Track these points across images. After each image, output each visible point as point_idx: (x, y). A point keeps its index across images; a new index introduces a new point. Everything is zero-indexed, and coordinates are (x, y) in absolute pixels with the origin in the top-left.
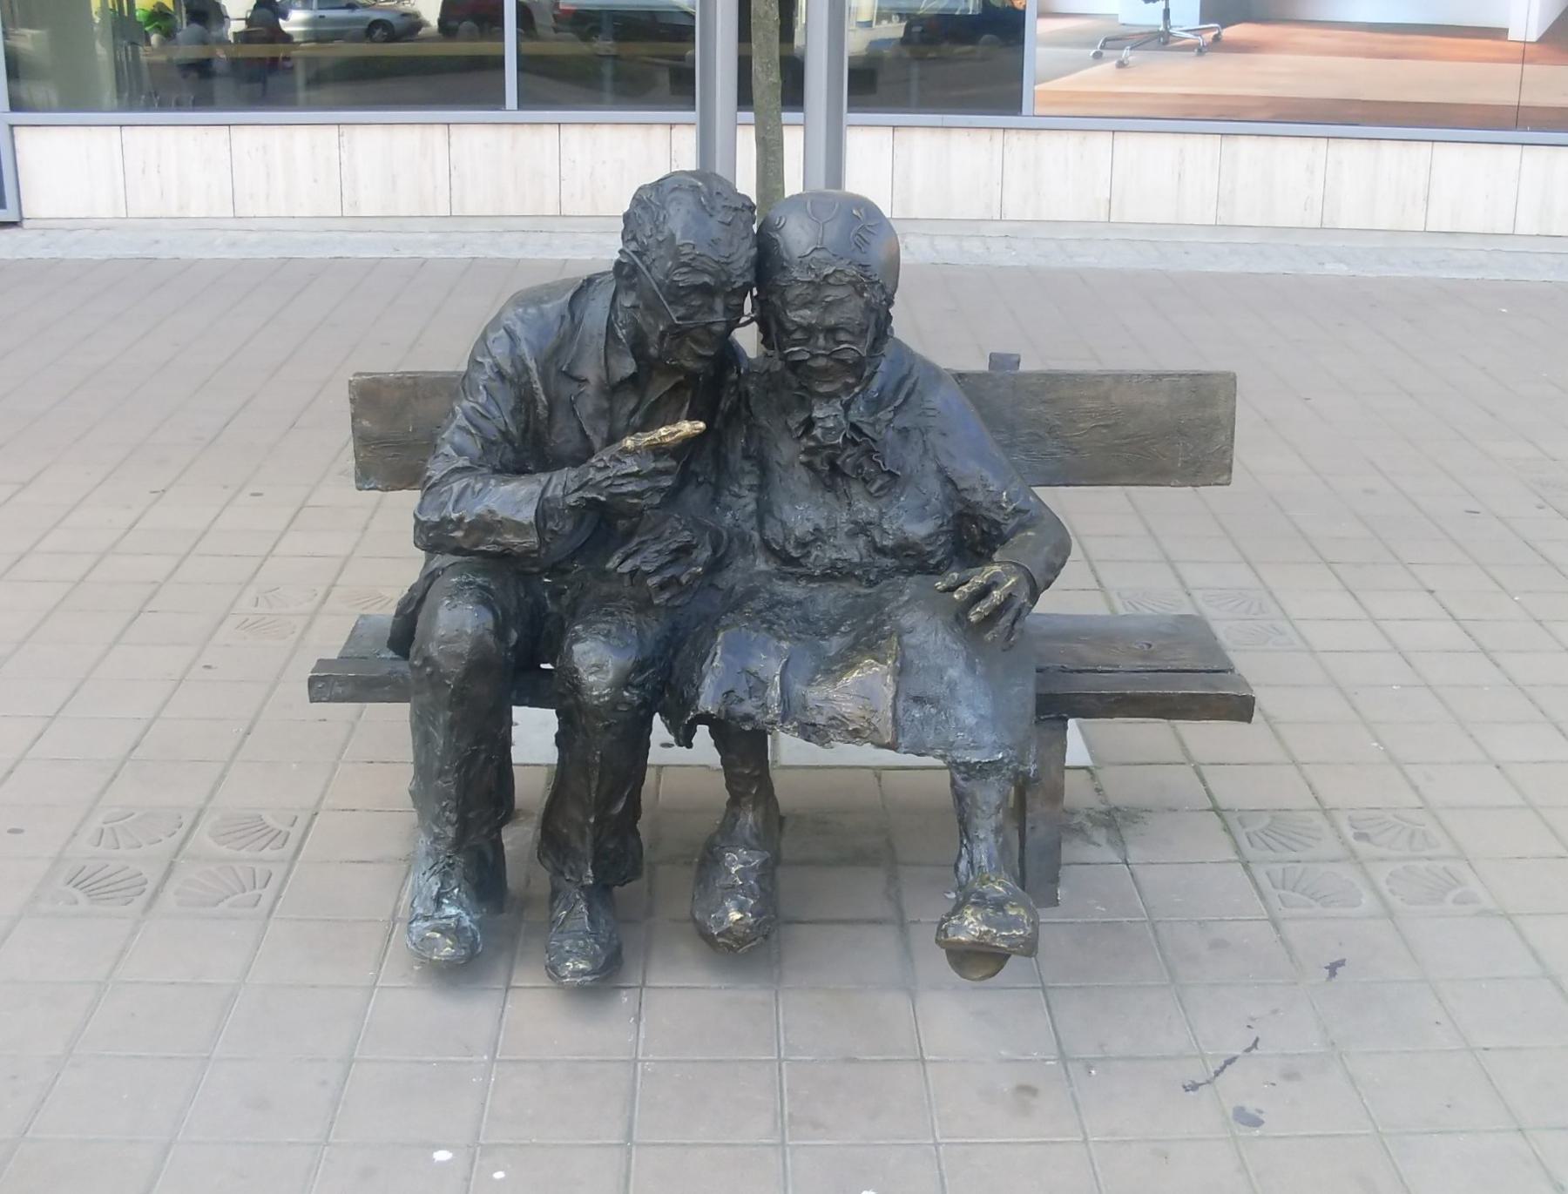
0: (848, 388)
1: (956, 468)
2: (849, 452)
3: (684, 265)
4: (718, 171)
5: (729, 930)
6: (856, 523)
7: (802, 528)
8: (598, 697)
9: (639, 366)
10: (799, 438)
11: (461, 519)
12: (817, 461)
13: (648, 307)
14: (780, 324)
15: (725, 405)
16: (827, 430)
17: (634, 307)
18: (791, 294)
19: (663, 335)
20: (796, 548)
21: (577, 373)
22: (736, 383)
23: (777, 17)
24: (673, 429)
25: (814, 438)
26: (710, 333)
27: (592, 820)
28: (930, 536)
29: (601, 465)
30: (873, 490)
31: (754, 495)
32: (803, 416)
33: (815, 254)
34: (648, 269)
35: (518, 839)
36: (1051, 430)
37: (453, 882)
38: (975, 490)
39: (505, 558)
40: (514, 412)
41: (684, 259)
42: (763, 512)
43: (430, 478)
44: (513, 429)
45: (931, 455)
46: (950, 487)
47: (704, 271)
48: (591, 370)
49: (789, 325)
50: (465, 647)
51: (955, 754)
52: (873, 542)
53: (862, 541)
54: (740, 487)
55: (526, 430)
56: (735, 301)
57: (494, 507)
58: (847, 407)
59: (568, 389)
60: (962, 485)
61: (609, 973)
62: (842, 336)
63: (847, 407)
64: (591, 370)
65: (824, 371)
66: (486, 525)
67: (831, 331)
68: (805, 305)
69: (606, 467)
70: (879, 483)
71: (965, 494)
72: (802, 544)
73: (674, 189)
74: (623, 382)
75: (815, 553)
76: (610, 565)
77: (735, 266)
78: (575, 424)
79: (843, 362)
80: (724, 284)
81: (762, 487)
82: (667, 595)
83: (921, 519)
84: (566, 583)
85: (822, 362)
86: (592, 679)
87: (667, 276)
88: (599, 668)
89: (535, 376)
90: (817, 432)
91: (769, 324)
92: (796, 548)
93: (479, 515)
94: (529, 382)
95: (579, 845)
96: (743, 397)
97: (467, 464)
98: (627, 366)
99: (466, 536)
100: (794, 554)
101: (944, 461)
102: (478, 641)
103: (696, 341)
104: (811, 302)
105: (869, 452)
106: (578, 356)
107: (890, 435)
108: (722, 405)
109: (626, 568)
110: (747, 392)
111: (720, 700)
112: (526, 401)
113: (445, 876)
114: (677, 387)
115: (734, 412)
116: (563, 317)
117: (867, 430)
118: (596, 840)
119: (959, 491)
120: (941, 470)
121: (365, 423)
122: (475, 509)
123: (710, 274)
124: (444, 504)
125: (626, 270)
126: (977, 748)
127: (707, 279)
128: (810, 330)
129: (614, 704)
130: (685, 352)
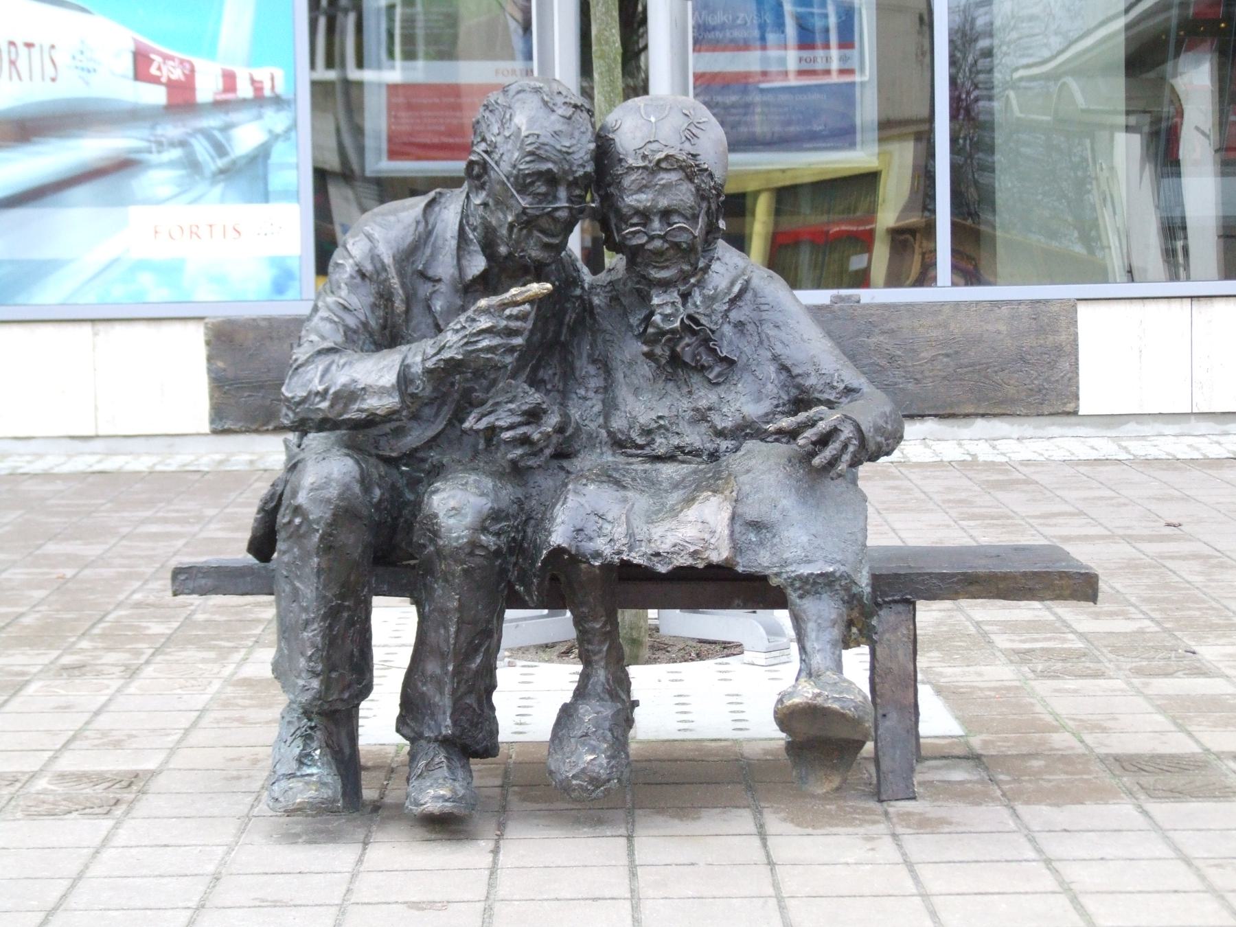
0: (685, 277)
1: (791, 354)
2: (687, 340)
3: (531, 153)
4: (557, 77)
5: (583, 770)
6: (697, 410)
7: (645, 418)
8: (458, 538)
11: (326, 391)
12: (658, 350)
13: (497, 203)
14: (618, 211)
15: (570, 318)
16: (666, 317)
17: (485, 205)
18: (626, 182)
19: (511, 227)
20: (641, 435)
21: (431, 273)
22: (580, 297)
23: (618, 44)
24: (523, 289)
27: (450, 668)
28: (767, 414)
29: (459, 326)
30: (711, 376)
31: (600, 396)
33: (649, 146)
34: (497, 163)
35: (378, 723)
36: (892, 359)
37: (315, 745)
38: (808, 375)
39: (371, 421)
40: (374, 307)
41: (529, 148)
42: (610, 407)
43: (296, 360)
44: (373, 323)
45: (766, 343)
46: (785, 373)
47: (547, 160)
48: (444, 268)
50: (333, 492)
51: (788, 569)
52: (713, 427)
53: (704, 427)
54: (587, 389)
55: (384, 327)
56: (577, 192)
57: (357, 376)
58: (685, 296)
59: (425, 289)
60: (795, 371)
62: (675, 218)
63: (685, 296)
64: (444, 268)
65: (659, 253)
66: (349, 395)
67: (666, 214)
68: (641, 190)
69: (464, 328)
70: (717, 370)
71: (799, 380)
72: (647, 432)
73: (518, 92)
74: (476, 280)
75: (658, 440)
76: (467, 425)
77: (576, 156)
78: (430, 321)
79: (677, 245)
80: (565, 173)
81: (607, 389)
82: (519, 452)
83: (758, 400)
84: (423, 471)
85: (658, 243)
86: (452, 521)
87: (514, 166)
88: (456, 511)
89: (392, 271)
90: (657, 318)
91: (609, 225)
92: (641, 435)
93: (344, 385)
94: (387, 279)
95: (437, 699)
96: (588, 309)
97: (332, 345)
98: (477, 264)
99: (332, 406)
100: (640, 441)
101: (779, 349)
102: (347, 487)
103: (543, 232)
104: (645, 186)
105: (706, 341)
106: (433, 256)
107: (727, 329)
108: (567, 319)
109: (482, 425)
110: (591, 303)
111: (570, 534)
112: (385, 297)
113: (307, 738)
115: (580, 321)
116: (418, 223)
117: (703, 320)
118: (454, 691)
119: (793, 377)
120: (775, 358)
121: (220, 364)
122: (340, 379)
123: (554, 162)
124: (310, 381)
125: (476, 169)
126: (809, 562)
127: (550, 165)
128: (645, 215)
129: (474, 545)
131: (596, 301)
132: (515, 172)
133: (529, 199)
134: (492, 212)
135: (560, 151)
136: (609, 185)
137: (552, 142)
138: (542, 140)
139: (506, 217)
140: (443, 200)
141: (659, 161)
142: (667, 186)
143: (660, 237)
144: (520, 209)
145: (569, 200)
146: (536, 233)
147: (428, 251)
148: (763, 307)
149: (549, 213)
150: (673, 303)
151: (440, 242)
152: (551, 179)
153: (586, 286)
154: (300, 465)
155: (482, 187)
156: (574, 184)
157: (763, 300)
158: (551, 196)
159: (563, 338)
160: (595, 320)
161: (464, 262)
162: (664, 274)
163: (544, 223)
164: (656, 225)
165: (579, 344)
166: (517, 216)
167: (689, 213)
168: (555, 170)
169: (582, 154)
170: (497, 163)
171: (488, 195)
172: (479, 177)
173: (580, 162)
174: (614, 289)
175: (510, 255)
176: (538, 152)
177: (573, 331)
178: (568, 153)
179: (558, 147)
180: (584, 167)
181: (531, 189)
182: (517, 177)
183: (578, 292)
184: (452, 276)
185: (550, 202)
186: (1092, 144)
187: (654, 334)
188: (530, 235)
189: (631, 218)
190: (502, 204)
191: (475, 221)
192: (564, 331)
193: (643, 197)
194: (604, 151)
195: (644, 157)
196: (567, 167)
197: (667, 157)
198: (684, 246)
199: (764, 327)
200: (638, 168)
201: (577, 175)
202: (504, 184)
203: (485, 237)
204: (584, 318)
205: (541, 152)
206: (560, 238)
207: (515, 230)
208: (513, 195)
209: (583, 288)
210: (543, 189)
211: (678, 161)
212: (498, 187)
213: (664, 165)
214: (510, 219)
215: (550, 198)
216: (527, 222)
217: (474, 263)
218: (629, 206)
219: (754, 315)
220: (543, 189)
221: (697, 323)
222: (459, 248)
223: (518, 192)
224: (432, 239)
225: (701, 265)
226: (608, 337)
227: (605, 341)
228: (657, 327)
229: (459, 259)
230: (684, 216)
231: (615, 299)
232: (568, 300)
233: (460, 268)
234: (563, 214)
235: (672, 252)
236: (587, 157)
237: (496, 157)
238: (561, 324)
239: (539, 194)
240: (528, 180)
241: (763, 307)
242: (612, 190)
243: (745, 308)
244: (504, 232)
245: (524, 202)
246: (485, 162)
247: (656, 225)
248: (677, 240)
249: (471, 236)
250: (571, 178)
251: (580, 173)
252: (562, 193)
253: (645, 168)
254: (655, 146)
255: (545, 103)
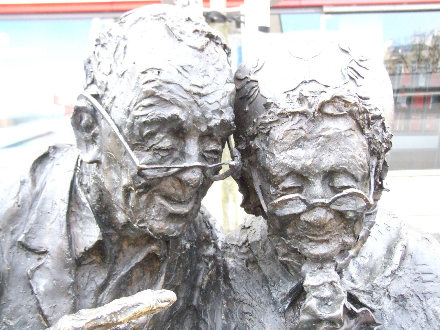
0: (344, 250)
3: (151, 95)
9: (105, 235)
10: (285, 312)
13: (110, 160)
14: (265, 172)
15: (203, 279)
16: (323, 301)
18: (277, 133)
21: (34, 244)
22: (213, 257)
25: (307, 310)
26: (183, 184)
32: (290, 286)
34: (108, 111)
41: (149, 87)
48: (51, 238)
49: (275, 171)
56: (212, 146)
61: (218, 238)
62: (342, 181)
64: (51, 238)
65: (320, 226)
67: (330, 175)
68: (298, 143)
74: (88, 252)
80: (196, 121)
85: (320, 214)
90: (311, 302)
91: (253, 183)
96: (222, 273)
98: (90, 234)
103: (167, 198)
104: (304, 138)
108: (200, 280)
110: (225, 266)
114: (152, 258)
115: (213, 285)
116: (23, 183)
117: (363, 299)
123: (181, 107)
125: (86, 118)
128: (302, 177)
130: (154, 212)
131: (230, 262)
132: (129, 121)
133: (148, 156)
134: (105, 172)
135: (187, 92)
136: (253, 137)
137: (177, 78)
138: (164, 76)
139: (120, 180)
140: (57, 155)
141: (323, 105)
142: (337, 138)
143: (323, 206)
144: (134, 172)
145: (202, 157)
146: (159, 200)
147: (33, 217)
148: (425, 277)
149: (174, 175)
150: (331, 283)
151: (48, 206)
152: (178, 130)
153: (220, 245)
154: (148, 162)
155: (93, 140)
156: (207, 136)
157: (424, 269)
158: (176, 152)
159: (195, 303)
160: (230, 285)
161: (76, 230)
162: (321, 250)
163: (169, 186)
164: (318, 190)
165: (213, 312)
166: (133, 178)
167: (359, 173)
168: (183, 117)
169: (218, 96)
170: (108, 111)
171: (100, 151)
172: (89, 128)
173: (216, 107)
174: (250, 251)
175: (127, 225)
176: (158, 93)
177: (205, 298)
178: (200, 95)
179: (188, 87)
180: (221, 113)
181: (151, 143)
182: (132, 127)
183: (211, 251)
184: (60, 248)
185: (175, 160)
186: (257, 111)
187: (308, 322)
188: (151, 199)
189: (282, 180)
190: (114, 162)
191: (88, 181)
192: (197, 294)
193: (298, 152)
194: (244, 97)
195: (302, 99)
196: (198, 114)
197: (335, 99)
198: (351, 215)
199: (430, 301)
200: (294, 114)
201: (212, 124)
202: (116, 136)
203: (100, 199)
204: (217, 282)
205: (163, 93)
206: (191, 205)
207: (133, 195)
208: (126, 152)
209: (216, 246)
210: (167, 143)
211: (347, 103)
212: (109, 140)
213: (329, 110)
214: (126, 181)
215: (176, 155)
216: (148, 187)
217: (87, 232)
218: (281, 164)
219: (417, 287)
220: (167, 143)
221: (359, 305)
222: (69, 213)
223: (133, 147)
224: (39, 203)
225: (362, 234)
226: (245, 308)
227: (243, 314)
228: (313, 314)
229: (69, 226)
230: (354, 178)
231: (252, 262)
232: (199, 261)
233: (71, 240)
234: (193, 176)
235: (334, 222)
236: (226, 101)
237: (106, 101)
238: (193, 287)
239: (160, 149)
240: (146, 131)
241: (425, 277)
242: (256, 143)
243: (405, 278)
244: (119, 197)
245: (140, 159)
246: (95, 110)
247: (318, 190)
248: (342, 208)
249: (84, 199)
250: (204, 128)
251: (216, 121)
252: (193, 147)
253: (304, 114)
254: (313, 87)
255: (170, 31)
